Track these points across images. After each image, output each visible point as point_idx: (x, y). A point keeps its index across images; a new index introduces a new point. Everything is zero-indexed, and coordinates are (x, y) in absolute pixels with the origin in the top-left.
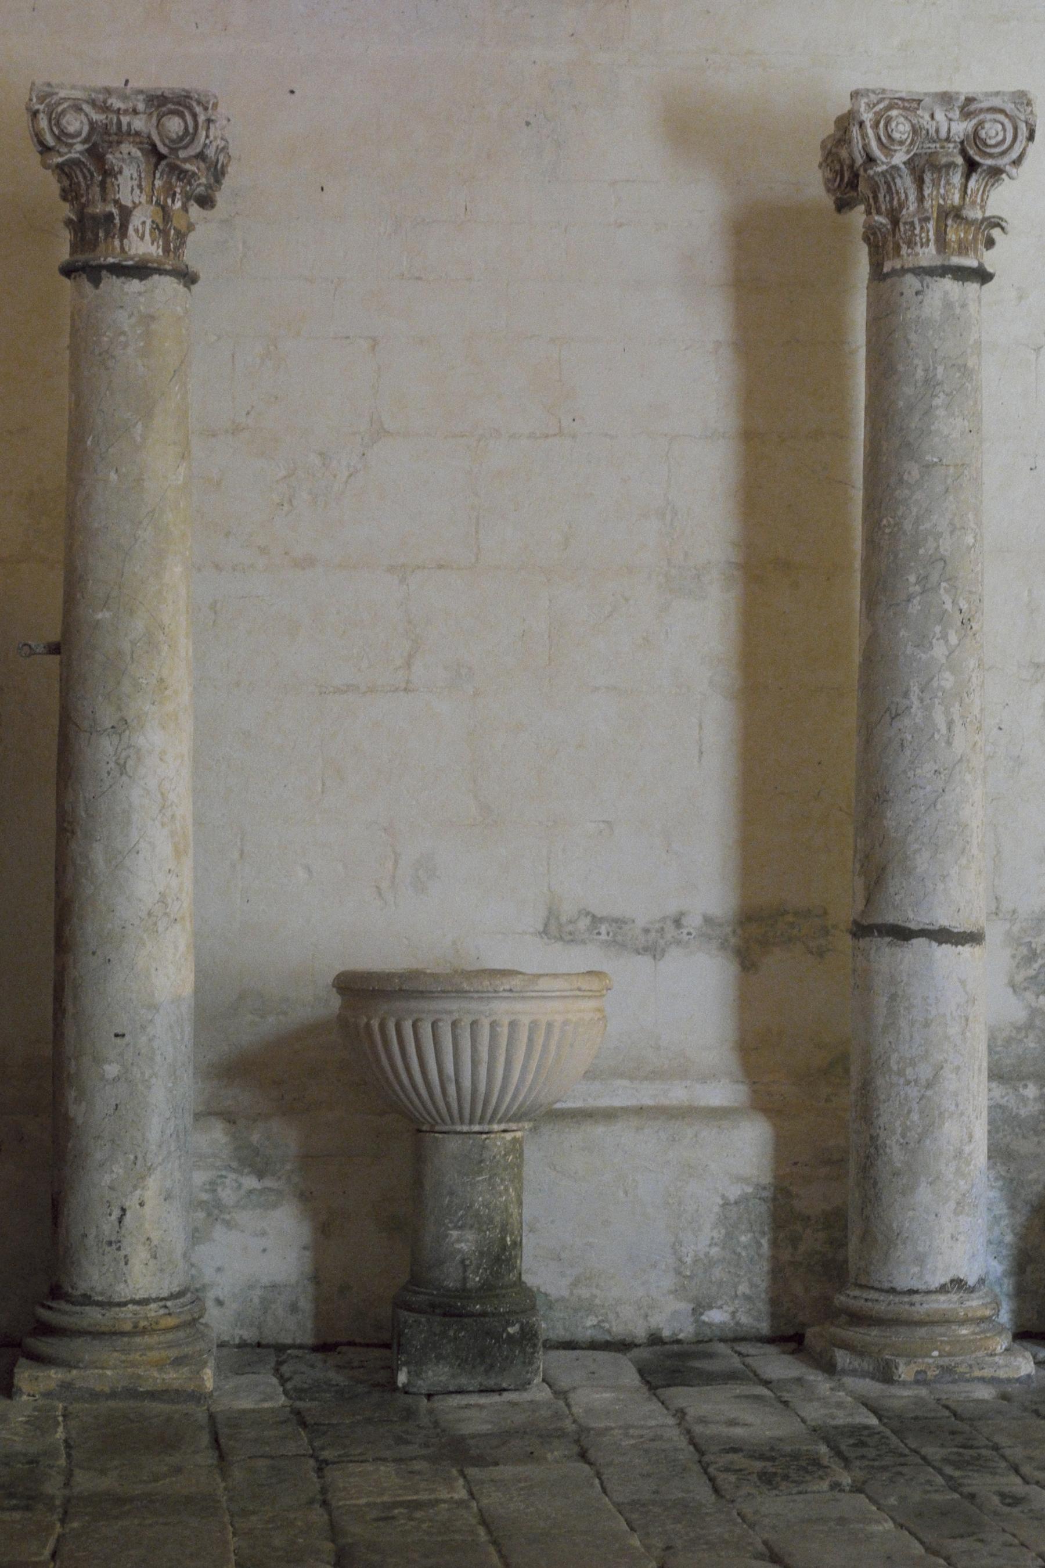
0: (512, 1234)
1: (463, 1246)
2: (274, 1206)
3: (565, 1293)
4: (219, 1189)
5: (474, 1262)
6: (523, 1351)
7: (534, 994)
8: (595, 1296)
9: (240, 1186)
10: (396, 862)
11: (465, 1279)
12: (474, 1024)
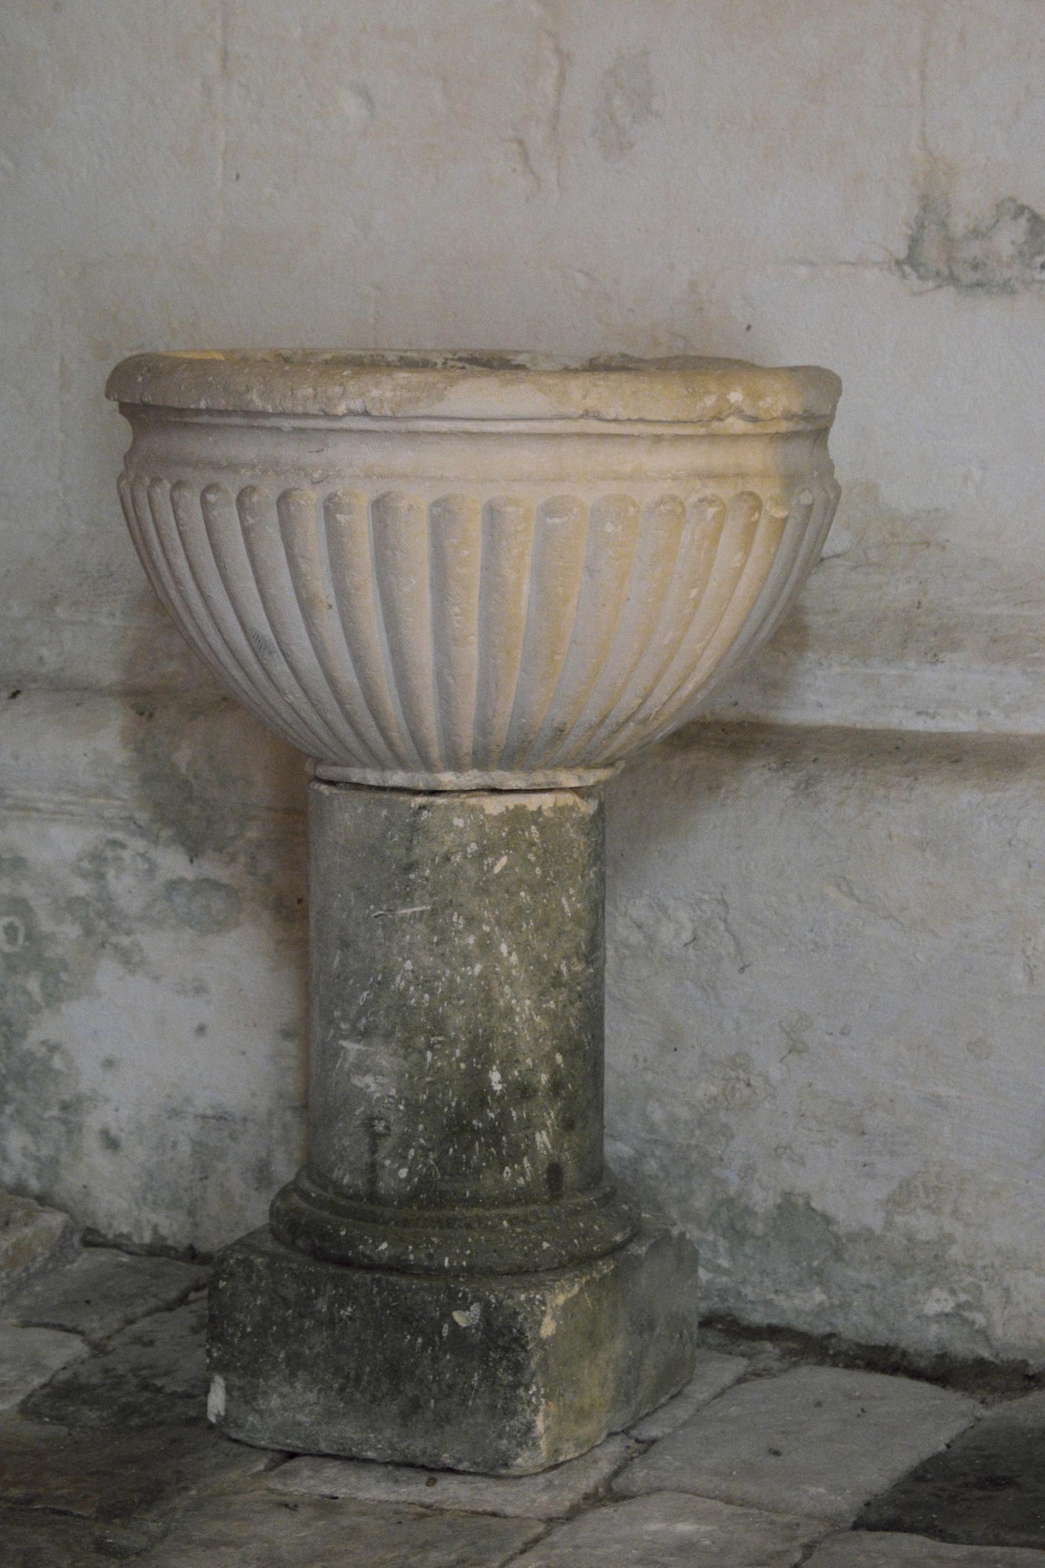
0: (508, 1062)
1: (368, 1082)
2: (220, 926)
3: (875, 1220)
4: (111, 874)
5: (394, 1128)
6: (490, 1377)
7: (445, 426)
8: (951, 1239)
9: (152, 870)
10: (562, 77)
11: (373, 1167)
12: (284, 499)
